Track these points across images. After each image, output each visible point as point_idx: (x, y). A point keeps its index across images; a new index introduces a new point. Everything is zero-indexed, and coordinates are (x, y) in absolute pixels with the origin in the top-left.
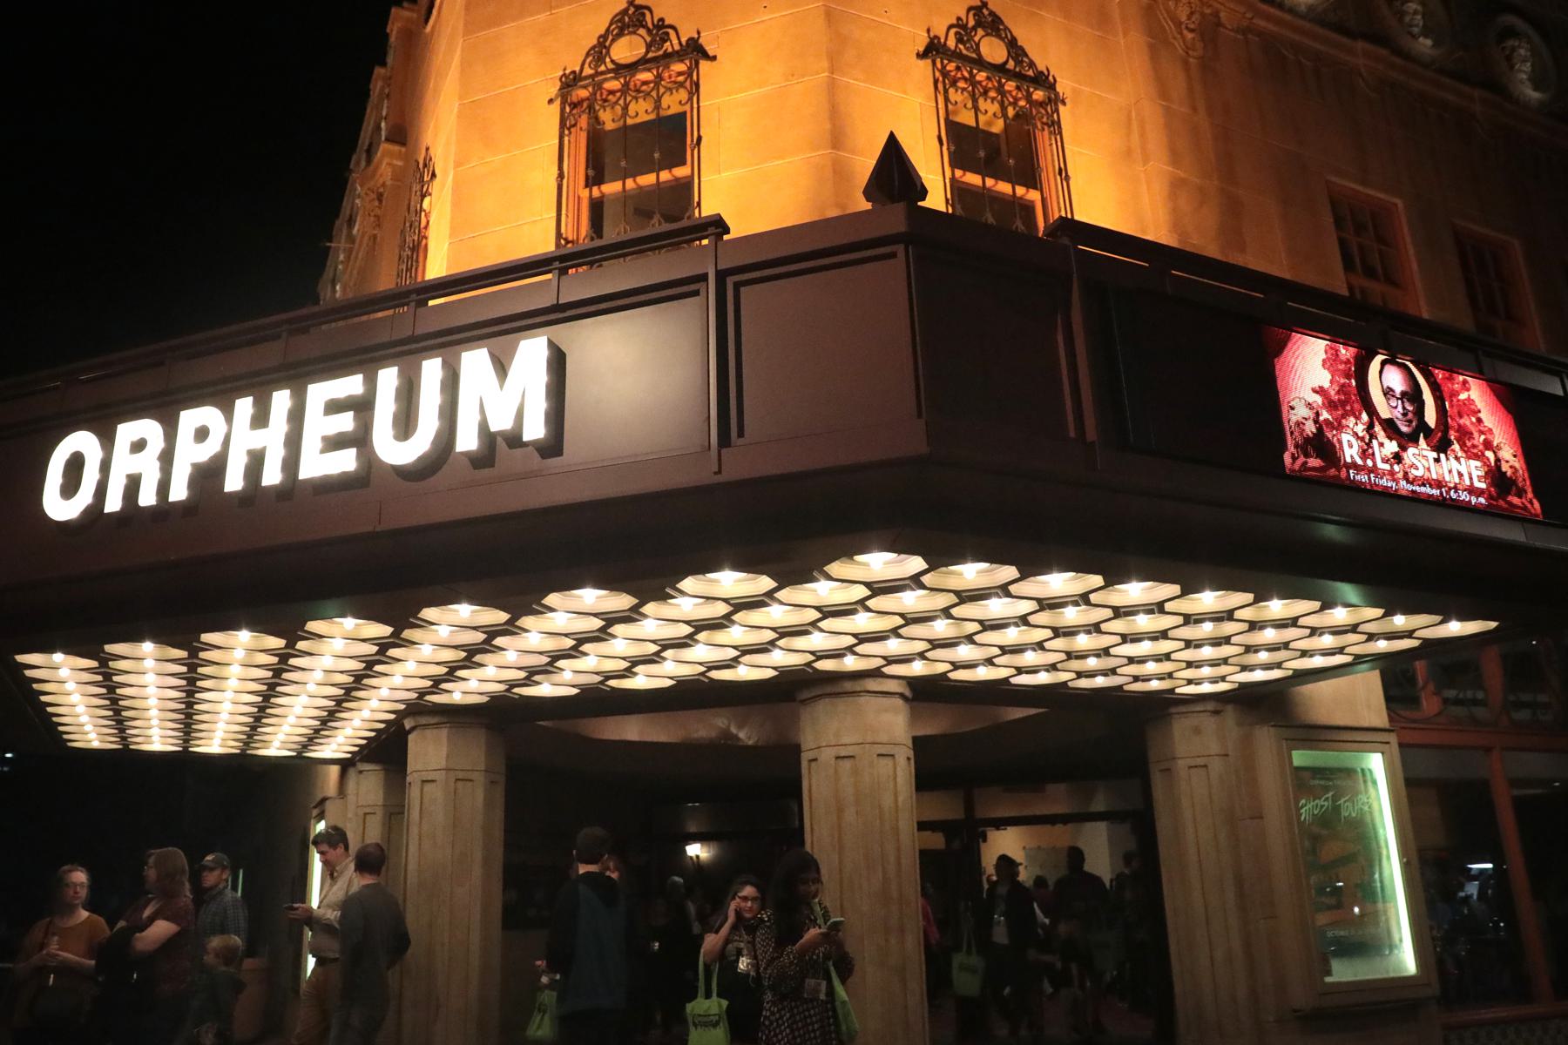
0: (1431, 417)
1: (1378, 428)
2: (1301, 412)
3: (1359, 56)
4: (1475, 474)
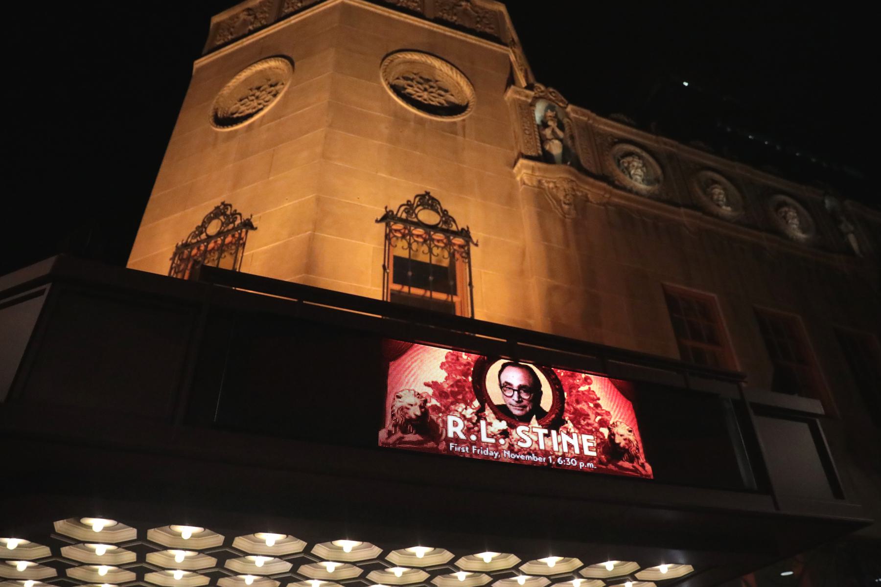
0: (547, 402)
1: (488, 412)
2: (408, 399)
3: (683, 216)
4: (586, 446)
